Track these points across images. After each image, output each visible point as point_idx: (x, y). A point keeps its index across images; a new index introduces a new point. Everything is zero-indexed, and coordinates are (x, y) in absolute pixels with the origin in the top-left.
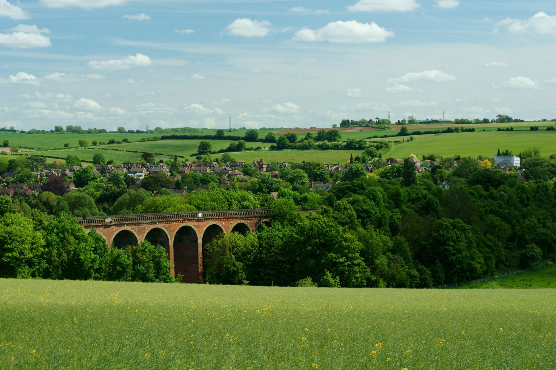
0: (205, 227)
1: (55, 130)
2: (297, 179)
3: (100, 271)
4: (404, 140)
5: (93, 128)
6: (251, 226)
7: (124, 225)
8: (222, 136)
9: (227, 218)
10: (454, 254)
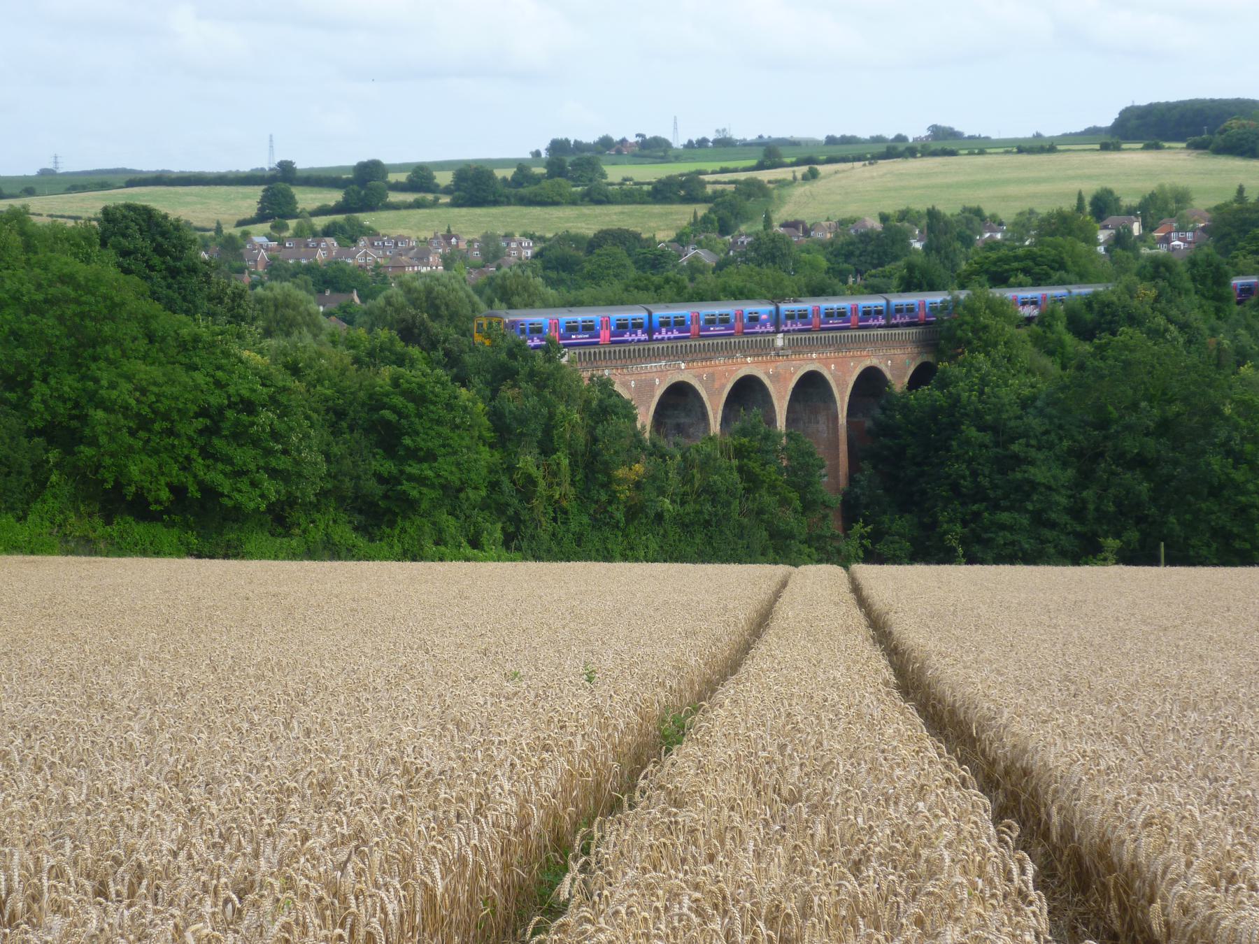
0: (791, 379)
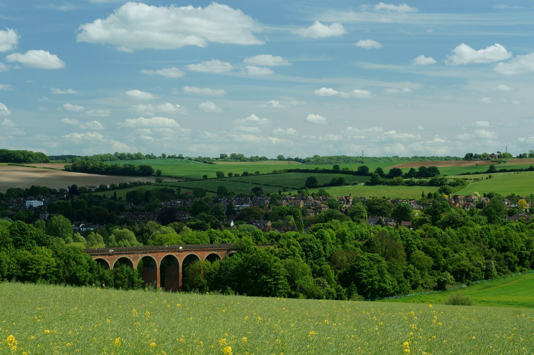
1: (221, 157)
2: (357, 214)
3: (365, 291)
4: (482, 178)
5: (254, 155)
6: (221, 256)
7: (123, 254)
8: (338, 170)
9: (202, 250)
10: (366, 278)
